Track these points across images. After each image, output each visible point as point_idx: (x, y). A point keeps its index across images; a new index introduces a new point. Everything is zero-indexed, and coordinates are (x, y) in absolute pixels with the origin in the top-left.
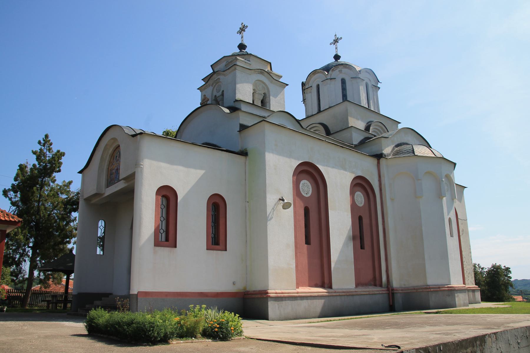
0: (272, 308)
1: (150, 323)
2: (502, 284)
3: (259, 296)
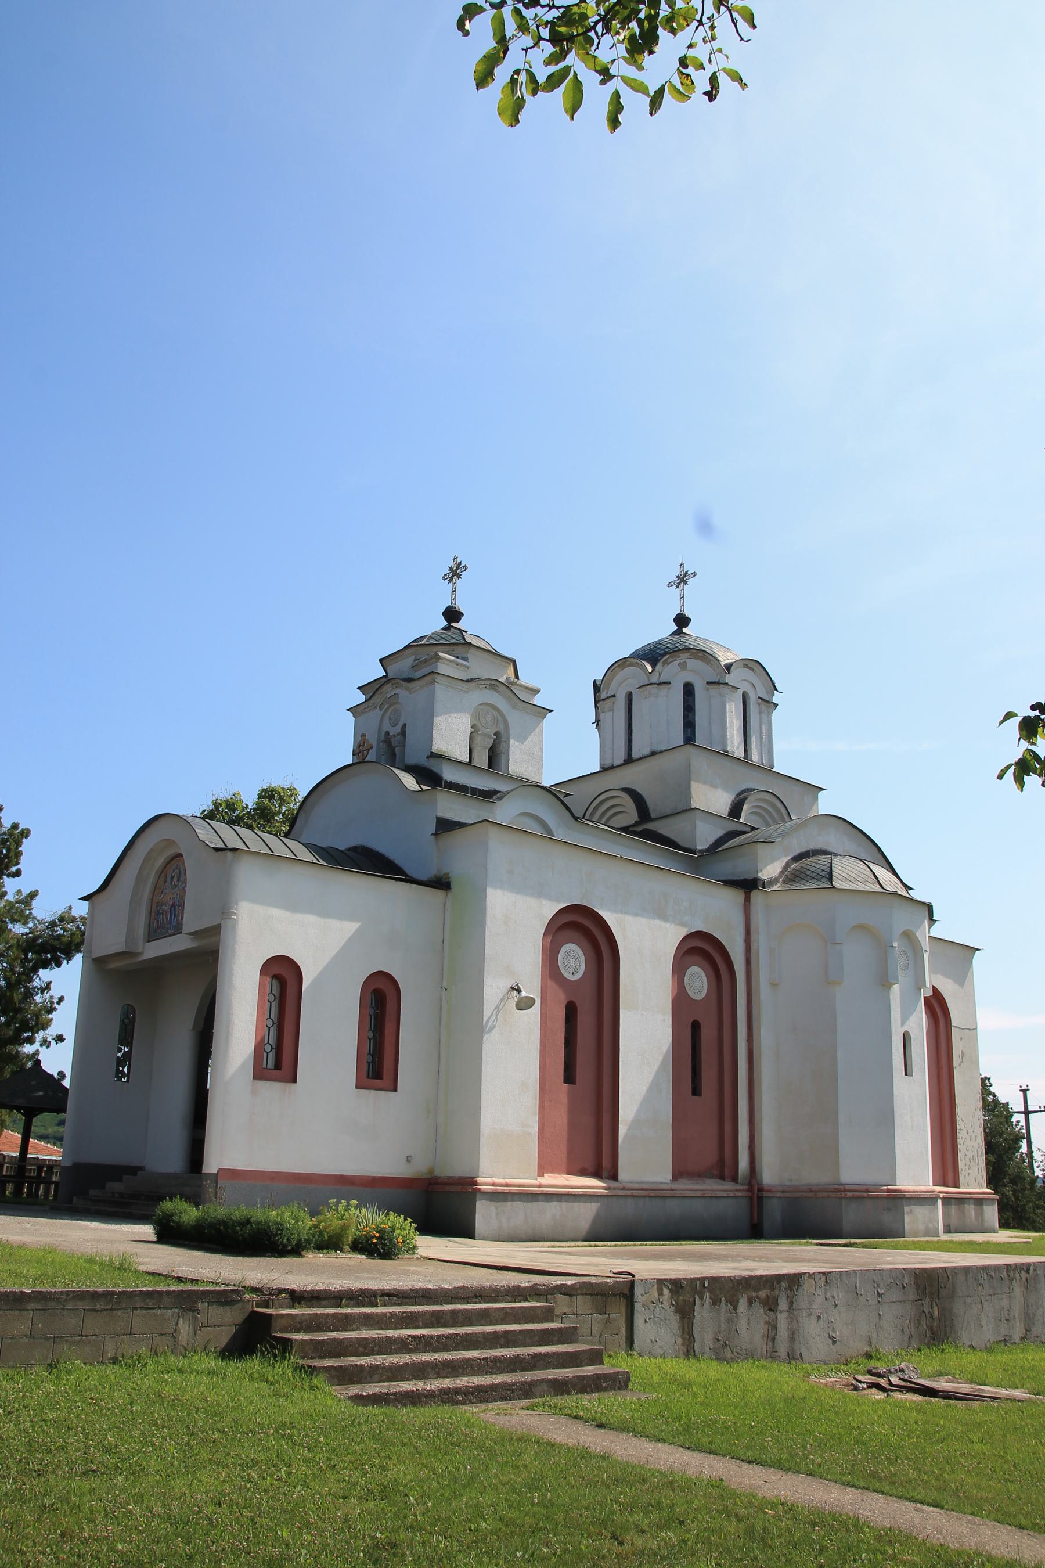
0: (484, 1214)
1: (277, 1223)
3: (458, 1188)
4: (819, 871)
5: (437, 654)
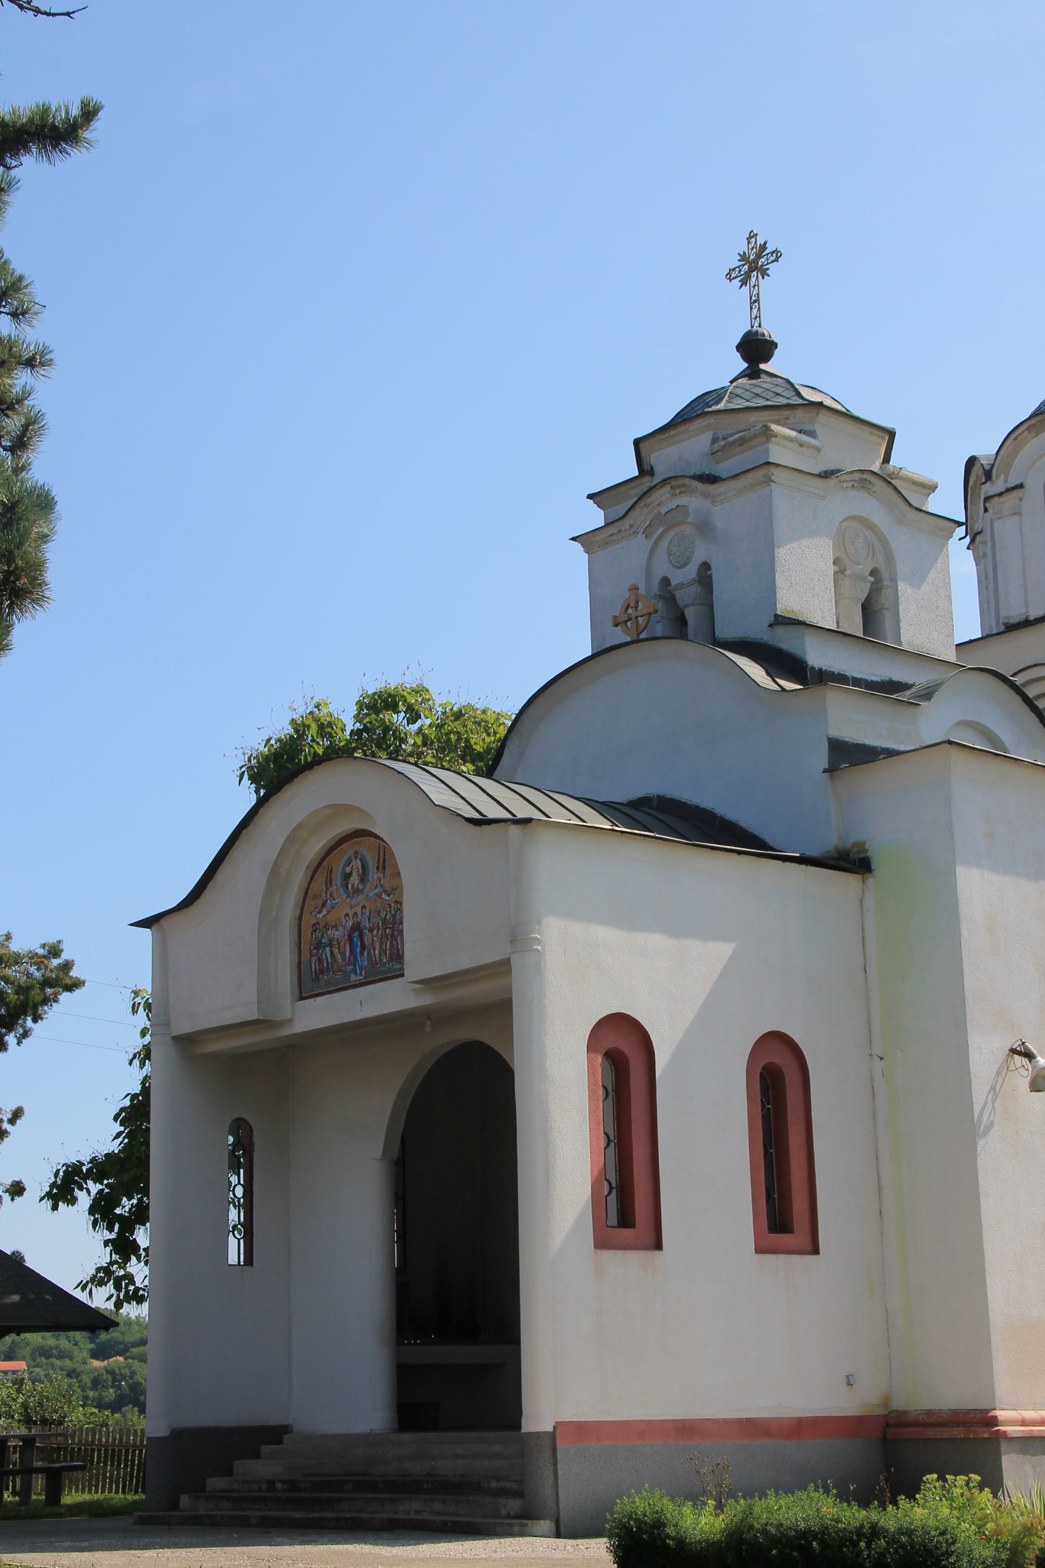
3: (958, 1432)
5: (767, 428)
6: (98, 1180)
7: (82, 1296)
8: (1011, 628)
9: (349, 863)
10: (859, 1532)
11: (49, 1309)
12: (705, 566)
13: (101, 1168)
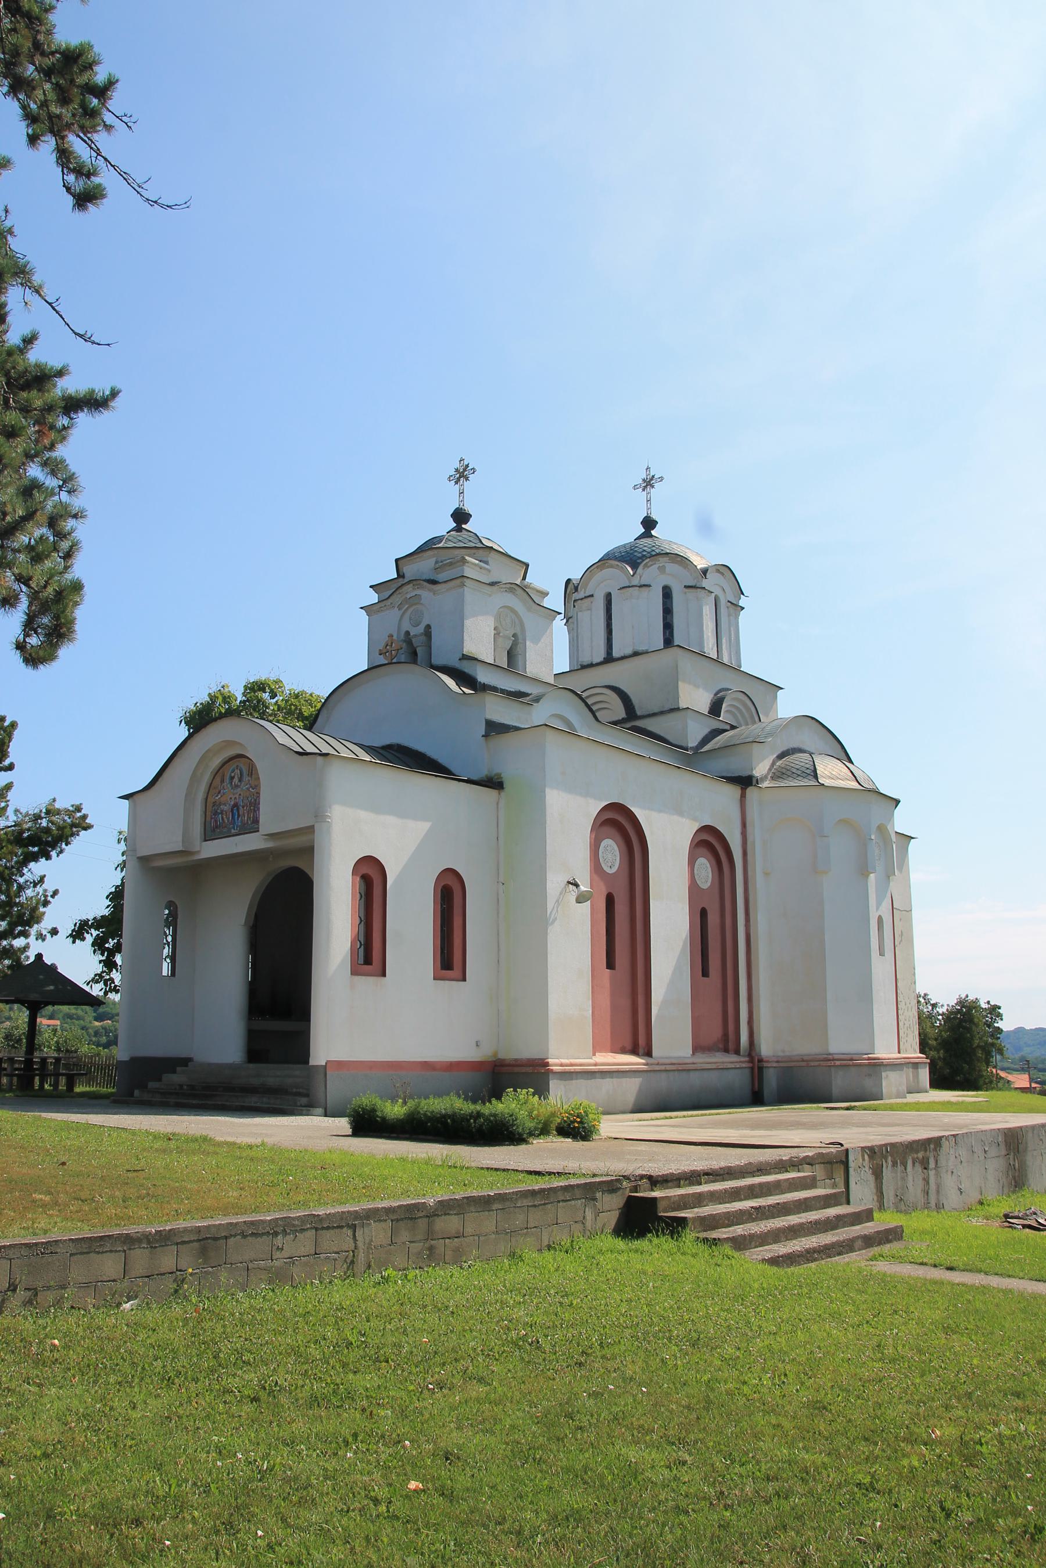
2: (978, 1046)
3: (529, 1070)
4: (804, 769)
6: (97, 929)
7: (87, 988)
8: (584, 667)
9: (233, 771)
10: (471, 1115)
11: (71, 994)
12: (428, 627)
13: (98, 923)
